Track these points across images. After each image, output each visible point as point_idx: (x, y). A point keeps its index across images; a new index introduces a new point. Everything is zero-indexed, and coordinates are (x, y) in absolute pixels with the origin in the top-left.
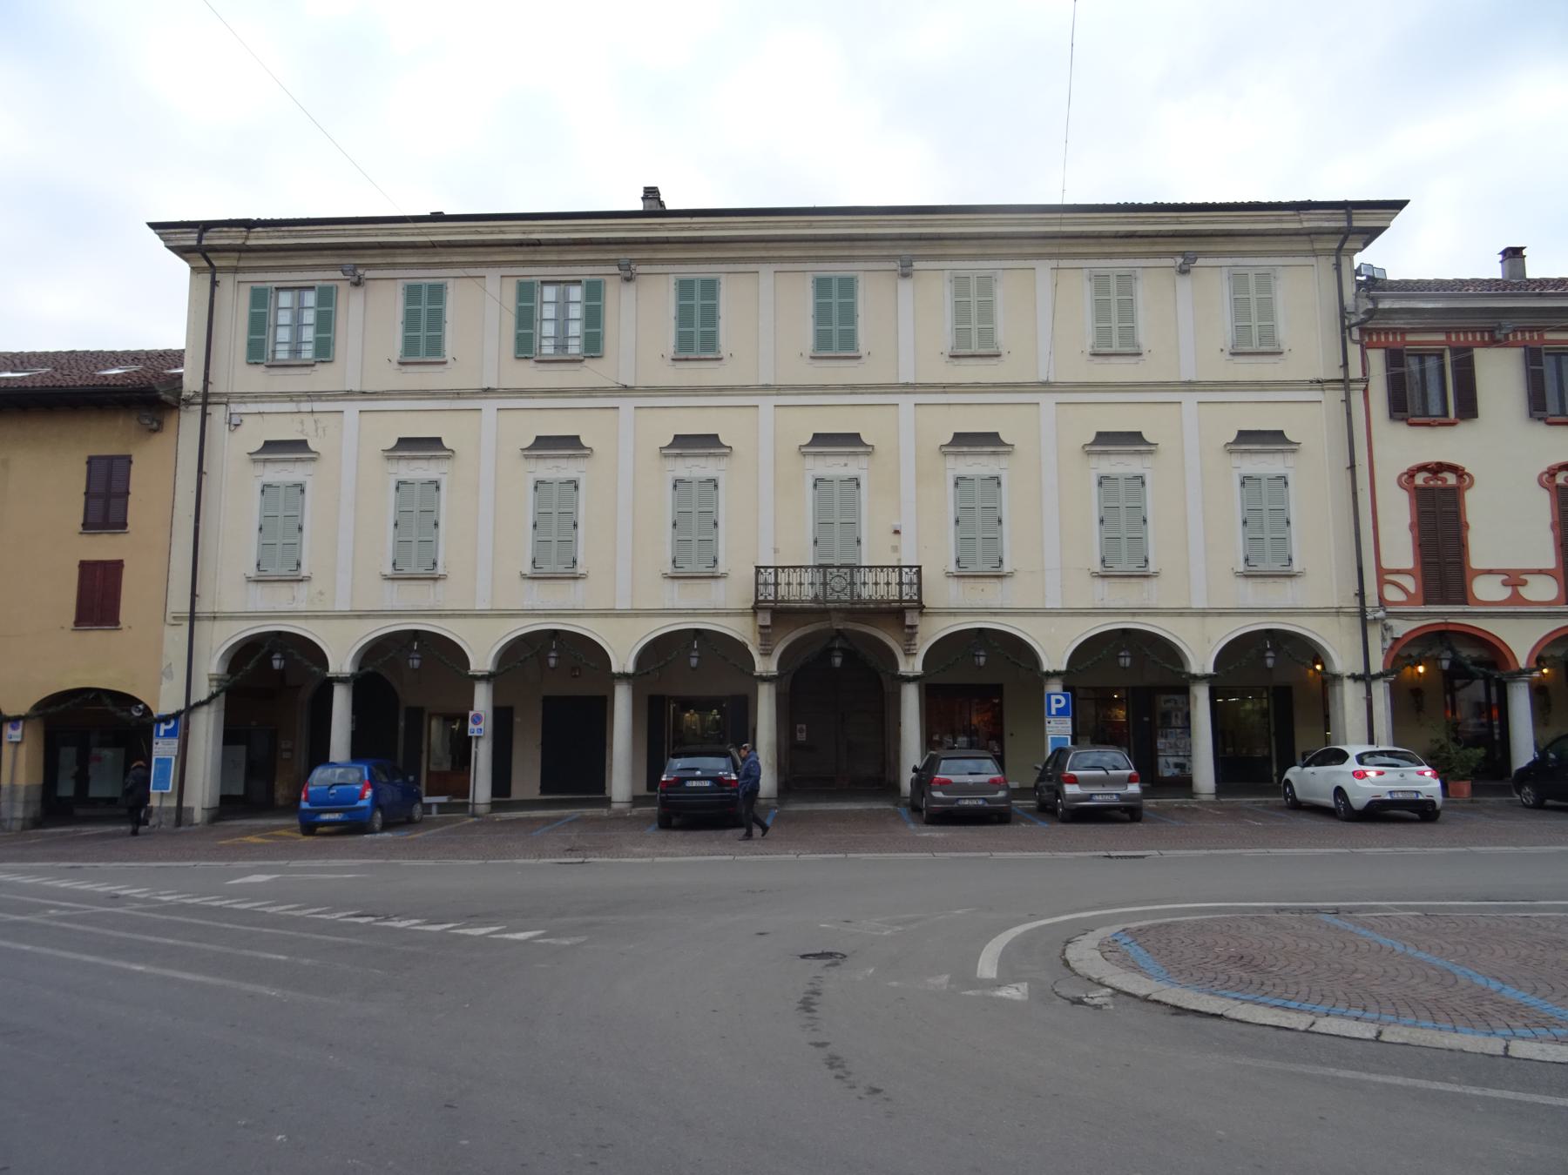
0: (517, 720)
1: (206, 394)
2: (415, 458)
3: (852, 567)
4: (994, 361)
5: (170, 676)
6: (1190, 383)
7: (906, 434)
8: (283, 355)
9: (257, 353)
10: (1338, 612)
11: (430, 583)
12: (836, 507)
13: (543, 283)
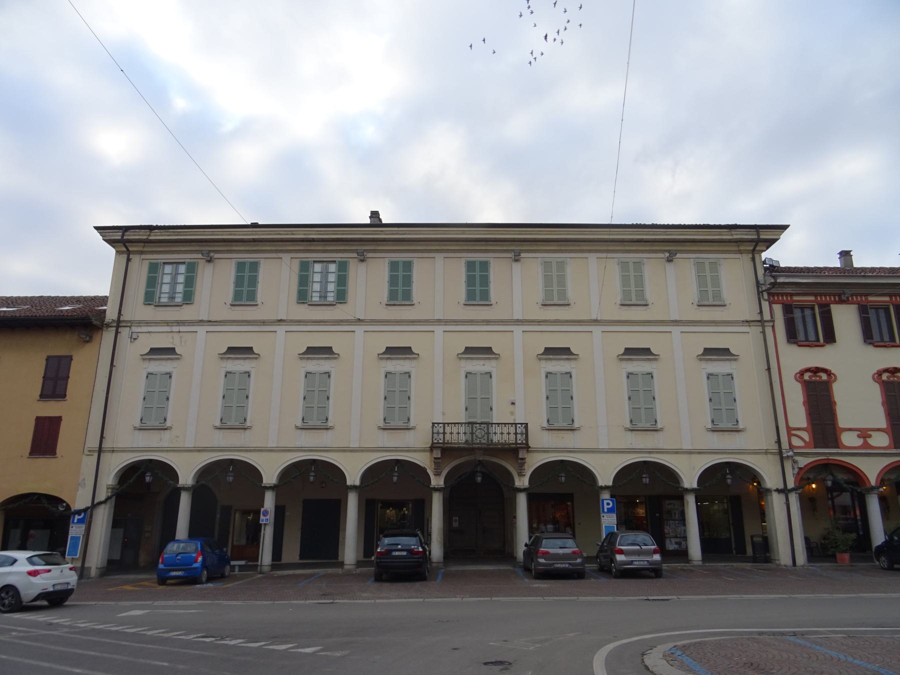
0: (287, 514)
1: (119, 321)
3: (488, 424)
4: (567, 308)
9: (150, 298)
10: (766, 452)
12: (478, 389)
13: (314, 262)
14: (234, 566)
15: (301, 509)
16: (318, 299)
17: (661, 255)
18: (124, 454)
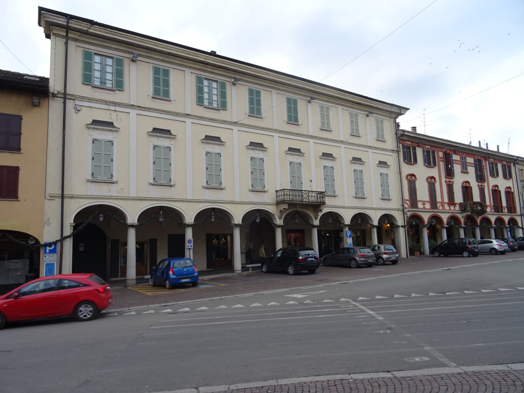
0: (158, 244)
1: (65, 94)
2: (161, 137)
4: (330, 133)
5: (49, 224)
6: (370, 146)
7: (312, 150)
8: (97, 83)
9: (87, 80)
10: (399, 210)
11: (169, 187)
12: (295, 170)
14: (249, 268)
15: (167, 241)
16: (207, 104)
17: (364, 113)
18: (81, 200)
